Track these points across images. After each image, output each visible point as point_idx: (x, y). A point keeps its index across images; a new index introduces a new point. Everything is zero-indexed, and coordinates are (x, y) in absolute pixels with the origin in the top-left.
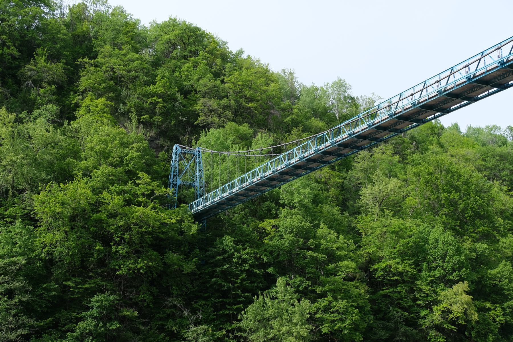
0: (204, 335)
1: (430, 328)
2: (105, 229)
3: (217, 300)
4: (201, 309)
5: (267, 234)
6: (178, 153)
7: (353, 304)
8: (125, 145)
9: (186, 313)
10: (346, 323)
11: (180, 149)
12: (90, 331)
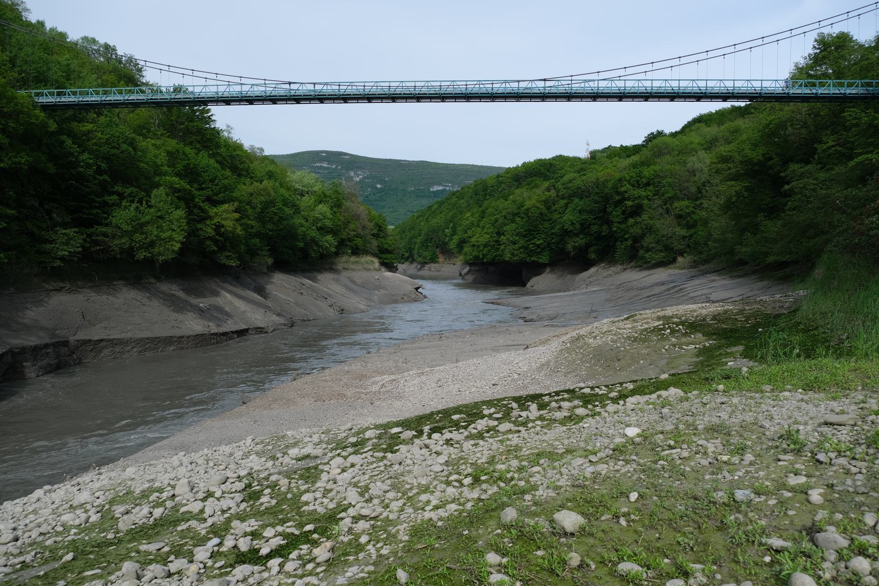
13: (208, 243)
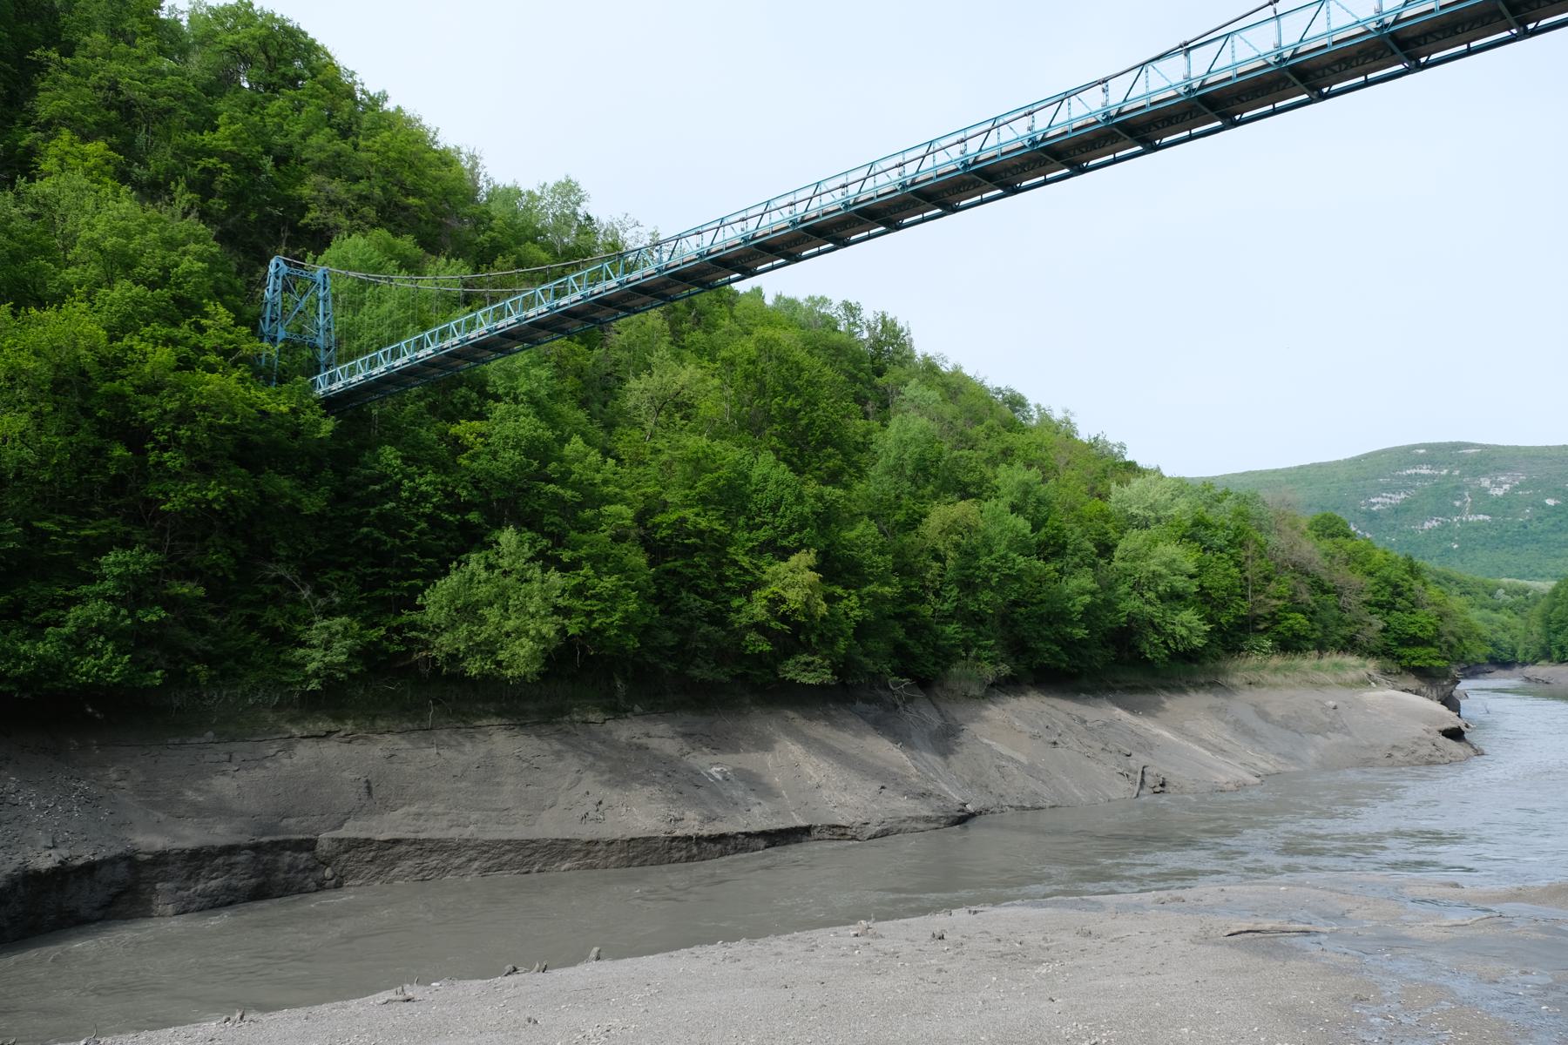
0: (345, 637)
1: (749, 628)
2: (135, 414)
3: (370, 571)
4: (336, 585)
5: (465, 449)
6: (281, 274)
7: (630, 582)
8: (170, 244)
9: (306, 594)
10: (615, 618)
11: (286, 268)
12: (100, 623)
13: (752, 636)
